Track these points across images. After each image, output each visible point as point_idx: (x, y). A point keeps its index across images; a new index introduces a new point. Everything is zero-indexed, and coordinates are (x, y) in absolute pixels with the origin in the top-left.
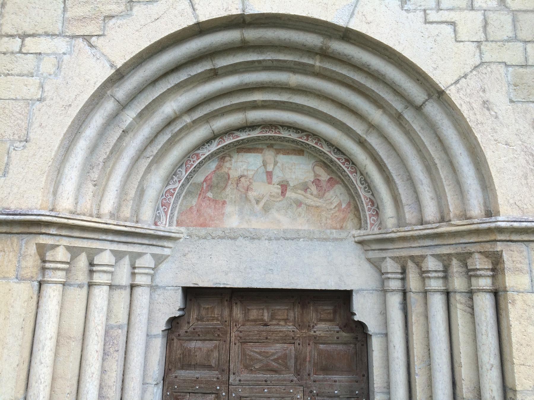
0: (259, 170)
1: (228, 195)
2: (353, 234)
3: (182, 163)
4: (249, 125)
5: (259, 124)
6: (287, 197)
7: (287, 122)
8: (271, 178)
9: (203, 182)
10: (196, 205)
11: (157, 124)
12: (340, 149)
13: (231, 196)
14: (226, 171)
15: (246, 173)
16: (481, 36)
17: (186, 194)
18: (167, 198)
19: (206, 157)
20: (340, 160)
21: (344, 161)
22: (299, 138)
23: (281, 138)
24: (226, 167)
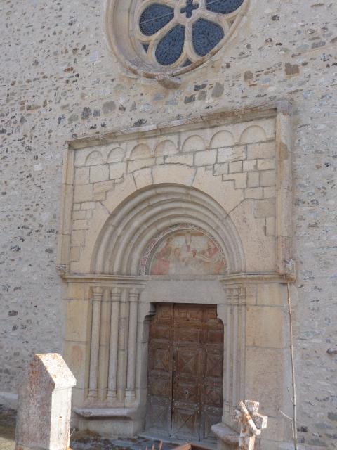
16: (245, 185)
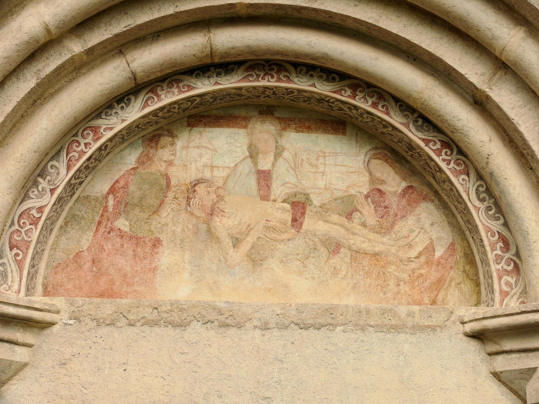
0: (240, 168)
1: (166, 225)
2: (460, 317)
3: (58, 147)
4: (216, 60)
5: (241, 58)
6: (306, 232)
7: (307, 55)
8: (268, 187)
9: (108, 194)
10: (89, 249)
11: (5, 55)
12: (431, 118)
13: (174, 228)
14: (162, 169)
15: (207, 174)
17: (66, 223)
18: (23, 231)
19: (115, 135)
20: (431, 145)
21: (438, 146)
22: (334, 92)
23: (293, 92)
24: (161, 160)
